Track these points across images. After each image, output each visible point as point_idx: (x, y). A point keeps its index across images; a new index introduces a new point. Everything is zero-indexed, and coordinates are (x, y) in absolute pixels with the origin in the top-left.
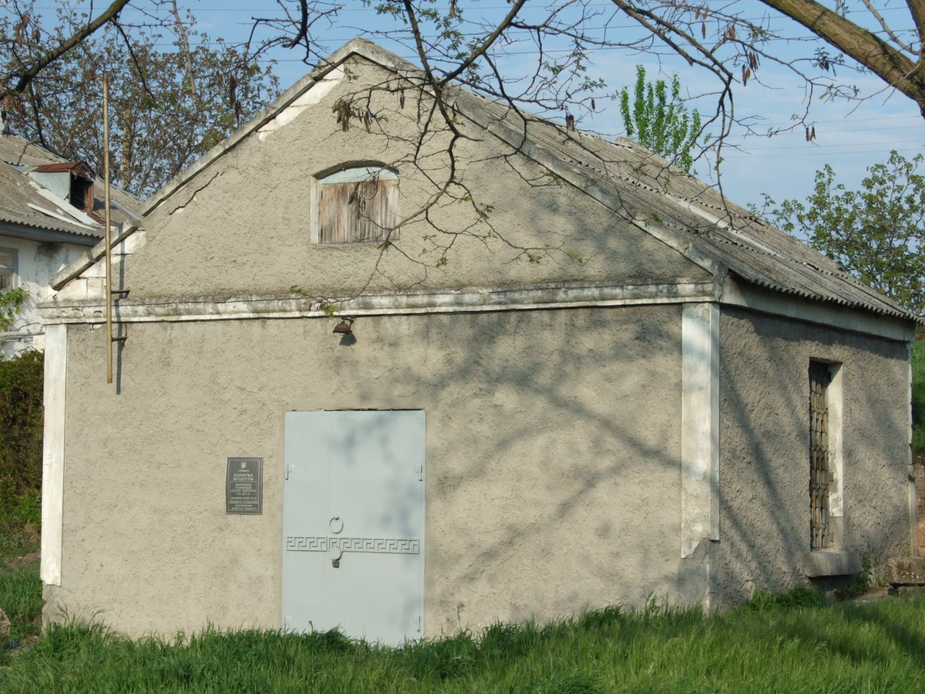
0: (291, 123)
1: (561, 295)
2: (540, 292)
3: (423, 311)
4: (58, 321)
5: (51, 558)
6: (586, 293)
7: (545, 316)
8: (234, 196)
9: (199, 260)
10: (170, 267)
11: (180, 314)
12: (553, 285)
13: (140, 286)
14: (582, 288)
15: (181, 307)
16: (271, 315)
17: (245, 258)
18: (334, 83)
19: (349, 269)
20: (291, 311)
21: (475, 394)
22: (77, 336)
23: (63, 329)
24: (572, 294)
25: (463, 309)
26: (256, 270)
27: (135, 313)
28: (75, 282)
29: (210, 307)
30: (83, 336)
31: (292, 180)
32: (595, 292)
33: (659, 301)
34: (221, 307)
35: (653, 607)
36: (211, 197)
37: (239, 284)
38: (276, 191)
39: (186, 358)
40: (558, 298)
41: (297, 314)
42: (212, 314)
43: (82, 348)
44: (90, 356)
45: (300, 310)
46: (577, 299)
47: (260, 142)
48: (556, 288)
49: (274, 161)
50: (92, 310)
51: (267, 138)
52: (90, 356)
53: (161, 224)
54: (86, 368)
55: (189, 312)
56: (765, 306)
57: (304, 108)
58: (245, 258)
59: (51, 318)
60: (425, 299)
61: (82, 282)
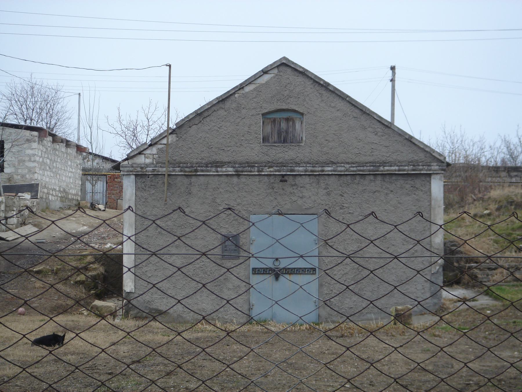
0: (251, 91)
1: (381, 168)
2: (372, 167)
3: (318, 173)
4: (131, 173)
5: (129, 280)
6: (393, 168)
7: (372, 177)
8: (223, 121)
9: (205, 148)
10: (190, 151)
11: (198, 172)
12: (378, 165)
13: (174, 158)
14: (391, 166)
15: (199, 168)
16: (243, 173)
17: (229, 149)
18: (273, 75)
19: (281, 155)
20: (254, 172)
21: (340, 208)
22: (141, 180)
23: (133, 177)
24: (386, 168)
25: (336, 173)
26: (234, 154)
27: (174, 171)
28: (139, 156)
29: (214, 169)
30: (144, 180)
31: (252, 115)
32: (397, 168)
33: (422, 172)
34: (219, 169)
35: (479, 164)
36: (211, 121)
37: (226, 160)
38: (244, 120)
39: (199, 191)
40: (380, 170)
41: (257, 173)
42: (214, 172)
43: (143, 185)
44: (147, 189)
45: (258, 172)
46: (388, 170)
47: (236, 98)
48: (380, 166)
49: (243, 107)
50: (151, 169)
51: (239, 97)
52: (147, 189)
53: (185, 131)
54: (146, 195)
55: (202, 171)
56: (136, 176)
57: (258, 85)
58: (229, 149)
59: (128, 171)
60: (320, 169)
61: (143, 156)
